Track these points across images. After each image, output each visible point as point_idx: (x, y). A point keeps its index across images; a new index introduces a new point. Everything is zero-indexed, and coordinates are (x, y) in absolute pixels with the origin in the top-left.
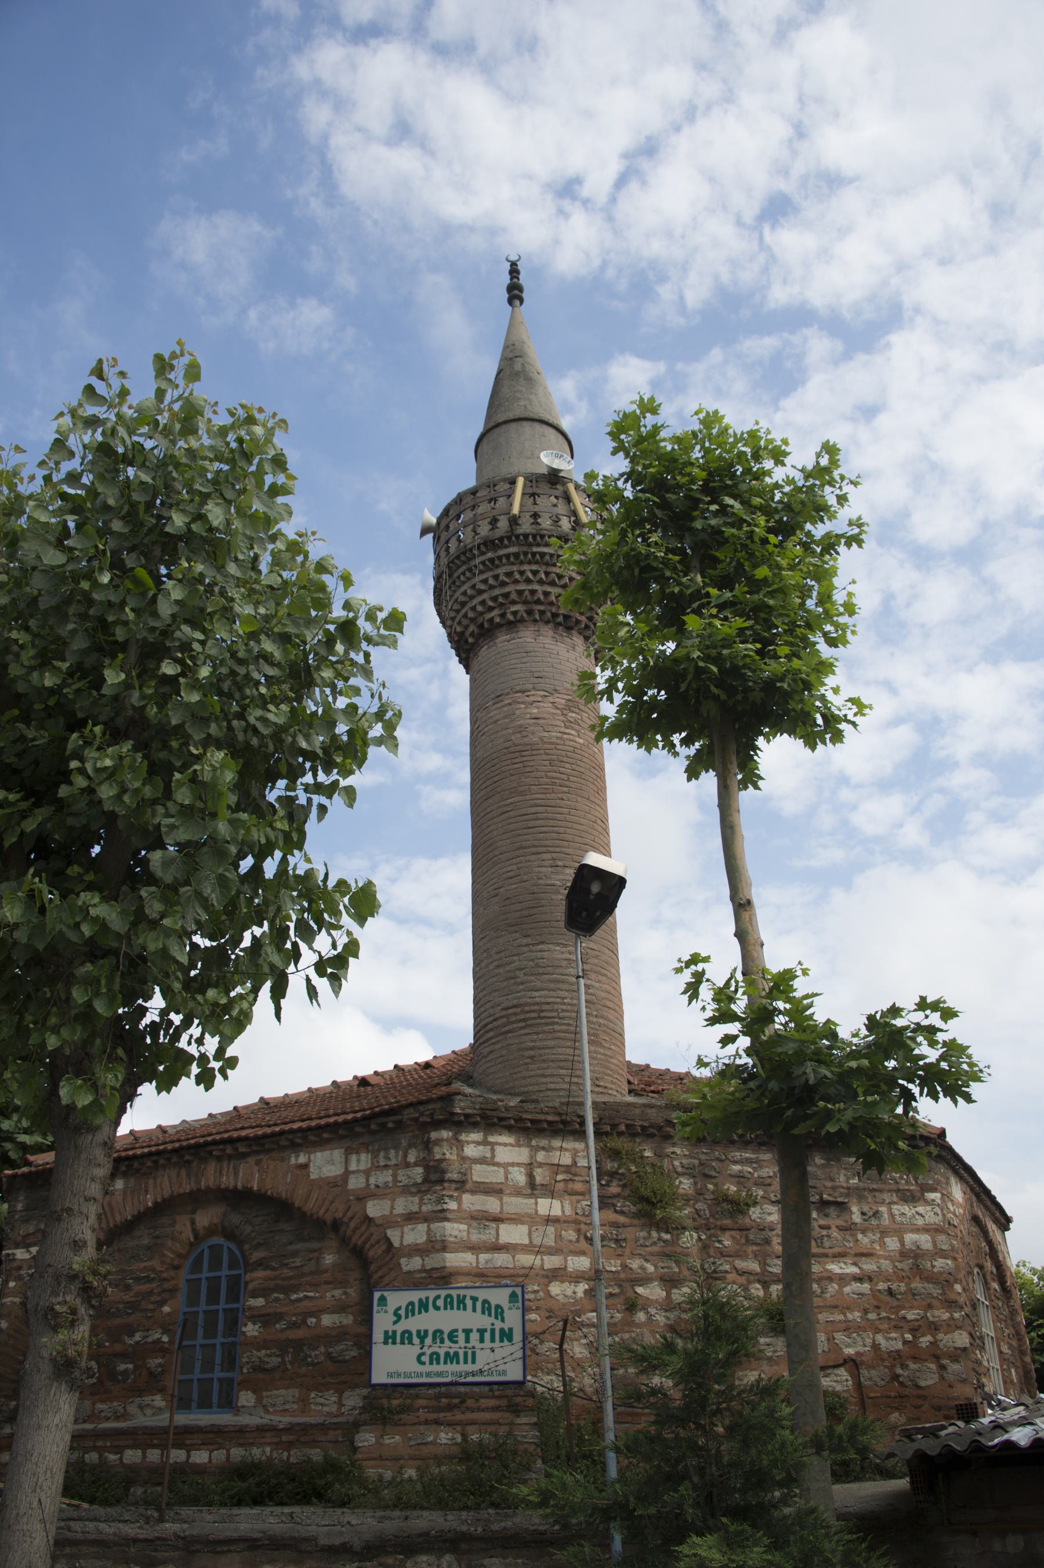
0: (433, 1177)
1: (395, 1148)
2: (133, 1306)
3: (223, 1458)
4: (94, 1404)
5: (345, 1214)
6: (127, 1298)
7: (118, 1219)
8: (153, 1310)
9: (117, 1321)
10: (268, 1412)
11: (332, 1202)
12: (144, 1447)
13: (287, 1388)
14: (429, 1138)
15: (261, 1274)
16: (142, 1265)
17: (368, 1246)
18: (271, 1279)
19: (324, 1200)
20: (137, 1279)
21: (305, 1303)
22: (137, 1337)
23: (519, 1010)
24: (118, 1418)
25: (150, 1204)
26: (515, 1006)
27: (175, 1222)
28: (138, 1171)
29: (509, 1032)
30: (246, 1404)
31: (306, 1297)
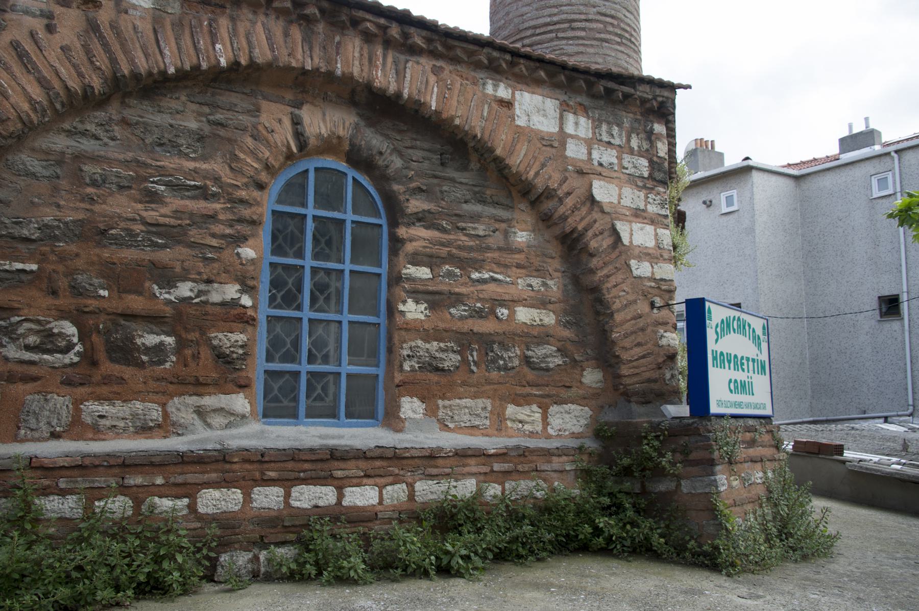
0: (659, 176)
1: (618, 125)
2: (171, 234)
3: (403, 497)
4: (77, 403)
5: (560, 185)
6: (151, 215)
8: (219, 249)
9: (129, 254)
10: (445, 427)
11: (543, 166)
13: (474, 397)
14: (652, 130)
15: (419, 231)
16: (191, 165)
17: (590, 233)
18: (443, 244)
20: (177, 188)
21: (492, 287)
22: (185, 289)
23: (616, 23)
24: (145, 430)
25: (223, 62)
26: (612, 17)
29: (606, 41)
30: (412, 415)
31: (494, 280)
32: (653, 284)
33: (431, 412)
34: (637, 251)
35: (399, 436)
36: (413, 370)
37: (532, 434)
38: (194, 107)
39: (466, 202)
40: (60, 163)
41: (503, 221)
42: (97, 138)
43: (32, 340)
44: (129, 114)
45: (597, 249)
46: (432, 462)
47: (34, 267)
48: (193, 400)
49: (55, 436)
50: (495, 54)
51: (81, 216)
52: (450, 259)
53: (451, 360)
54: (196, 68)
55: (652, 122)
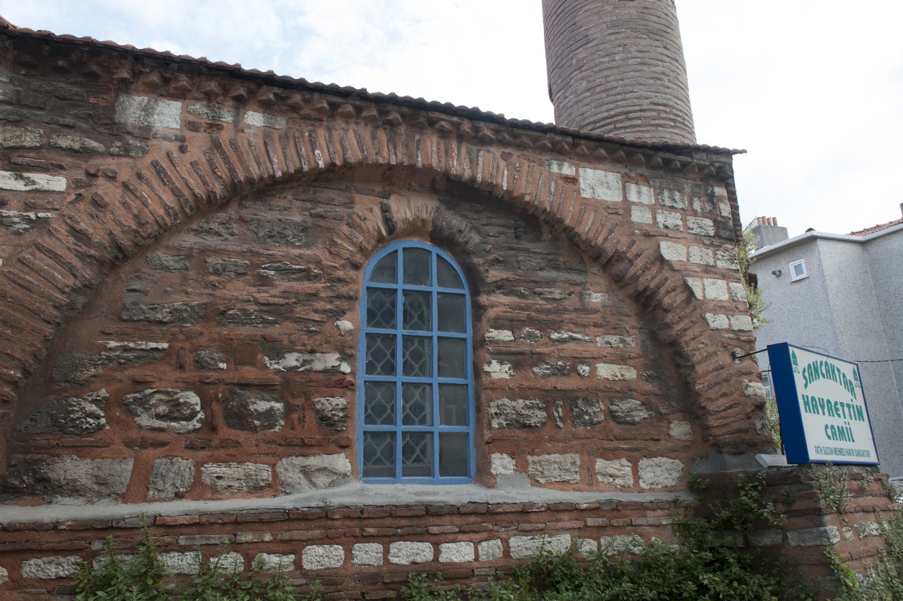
1: (679, 191)
3: (499, 553)
4: (198, 465)
5: (629, 248)
6: (263, 296)
7: (255, 171)
9: (245, 331)
10: (536, 483)
11: (611, 231)
12: (348, 540)
13: (563, 452)
16: (296, 252)
18: (522, 309)
19: (603, 225)
20: (284, 272)
21: (571, 346)
22: (292, 360)
24: (257, 489)
25: (321, 164)
26: (664, 105)
27: (352, 202)
28: (295, 108)
30: (503, 471)
32: (732, 336)
33: (521, 467)
34: (711, 305)
35: (492, 492)
36: (501, 427)
37: (624, 489)
38: (299, 204)
39: (541, 269)
40: (189, 257)
41: (577, 284)
42: (218, 234)
43: (162, 409)
44: (247, 213)
45: (671, 305)
46: (525, 518)
47: (166, 345)
48: (299, 461)
49: (179, 496)
50: (558, 138)
51: (205, 300)
52: (530, 321)
53: (538, 416)
54: (299, 171)
55: (713, 186)
